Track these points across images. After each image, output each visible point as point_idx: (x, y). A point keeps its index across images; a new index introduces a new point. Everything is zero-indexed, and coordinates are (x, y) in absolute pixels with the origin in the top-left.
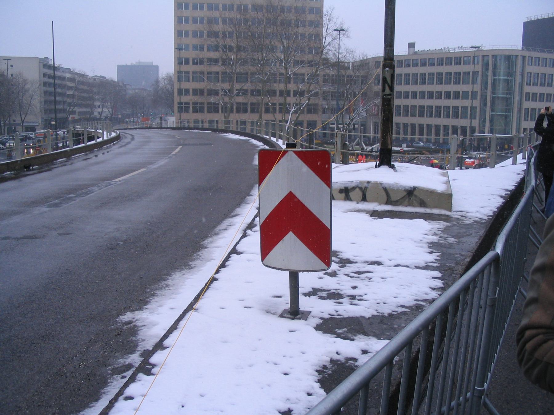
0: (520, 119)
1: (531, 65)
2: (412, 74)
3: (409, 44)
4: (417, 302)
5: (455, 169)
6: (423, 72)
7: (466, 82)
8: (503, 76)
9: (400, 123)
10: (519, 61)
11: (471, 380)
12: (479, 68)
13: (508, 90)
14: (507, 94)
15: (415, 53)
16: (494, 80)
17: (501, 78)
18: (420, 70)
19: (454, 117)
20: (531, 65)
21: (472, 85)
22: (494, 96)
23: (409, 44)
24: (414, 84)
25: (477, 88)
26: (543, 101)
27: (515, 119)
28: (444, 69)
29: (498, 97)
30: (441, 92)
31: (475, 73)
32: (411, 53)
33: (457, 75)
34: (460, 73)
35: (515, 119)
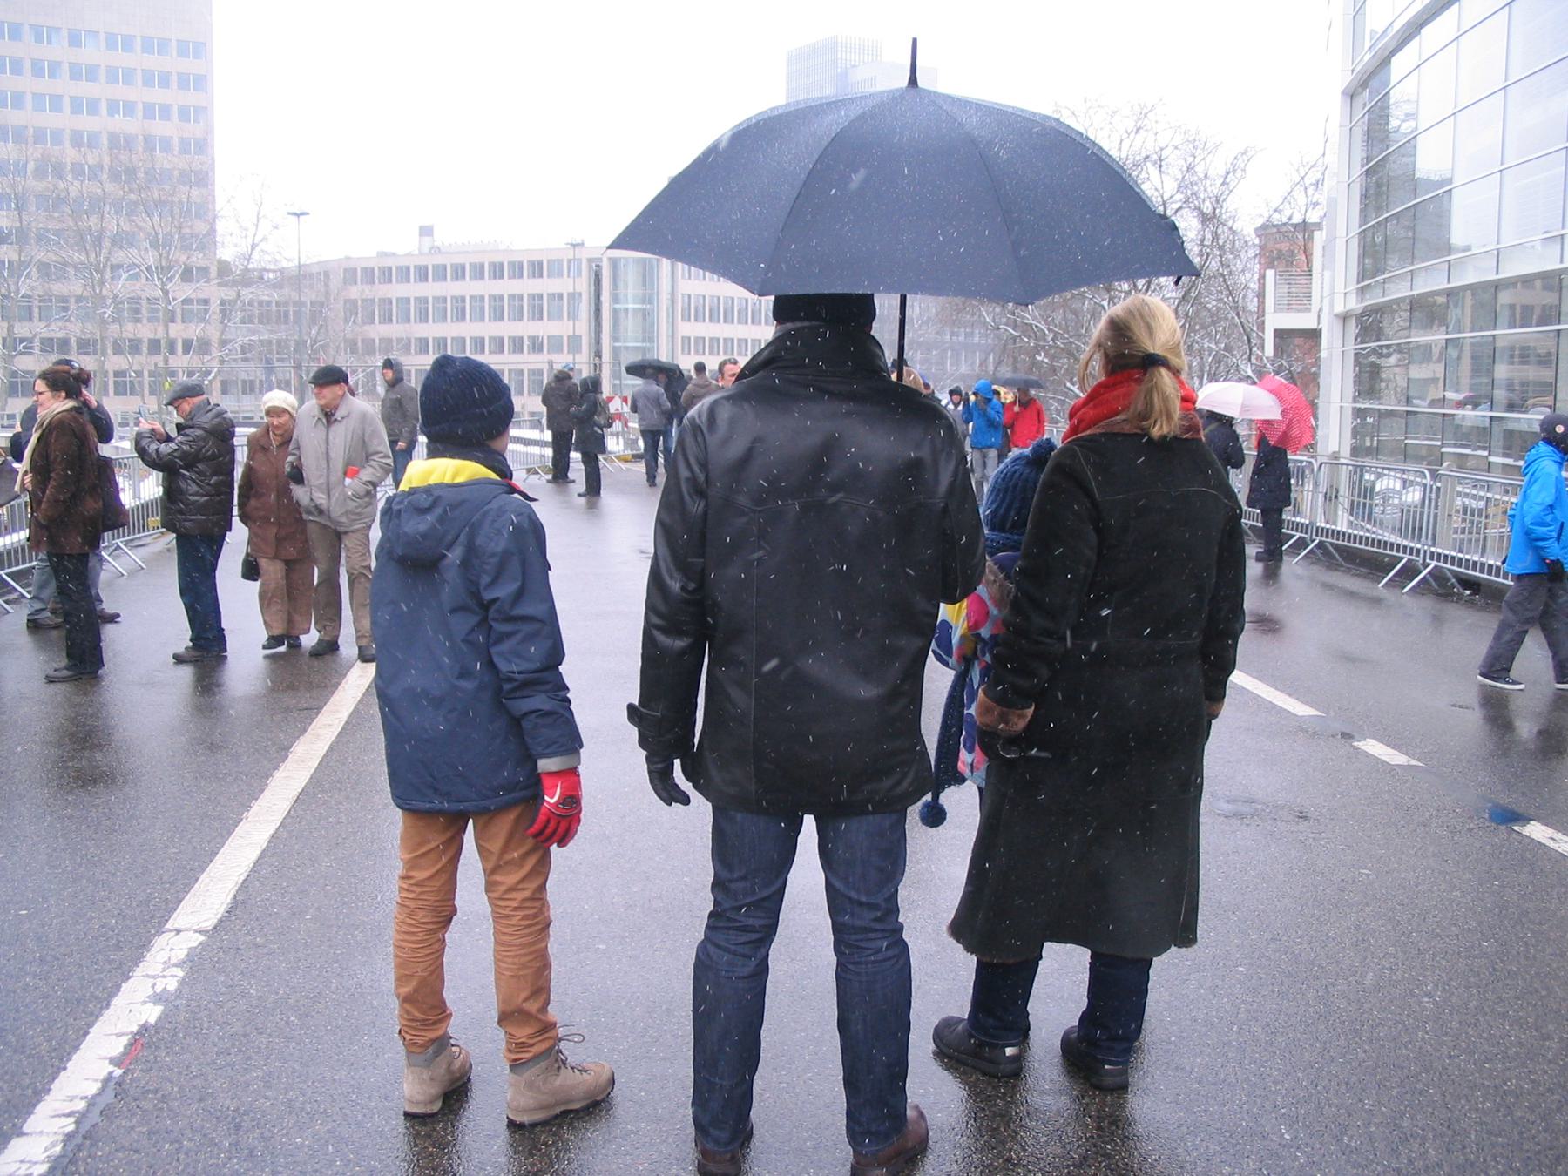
0: (673, 312)
1: (690, 278)
2: (434, 298)
3: (421, 228)
4: (48, 1153)
5: (671, 805)
6: (458, 293)
7: (556, 316)
8: (634, 303)
9: (171, 40)
10: (664, 280)
11: (735, 951)
12: (584, 286)
13: (644, 331)
14: (644, 340)
15: (436, 250)
16: (615, 310)
17: (631, 306)
18: (452, 288)
19: (534, 392)
20: (690, 278)
21: (571, 323)
22: (617, 344)
23: (421, 228)
24: (439, 321)
25: (583, 327)
26: (725, 339)
27: (663, 314)
28: (507, 287)
29: (627, 348)
30: (501, 340)
31: (575, 297)
32: (426, 250)
33: (534, 299)
34: (541, 297)
35: (663, 314)
